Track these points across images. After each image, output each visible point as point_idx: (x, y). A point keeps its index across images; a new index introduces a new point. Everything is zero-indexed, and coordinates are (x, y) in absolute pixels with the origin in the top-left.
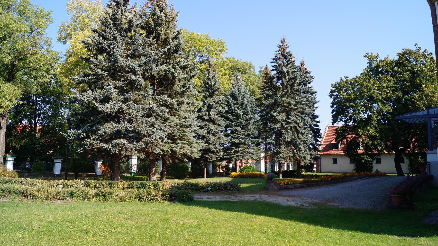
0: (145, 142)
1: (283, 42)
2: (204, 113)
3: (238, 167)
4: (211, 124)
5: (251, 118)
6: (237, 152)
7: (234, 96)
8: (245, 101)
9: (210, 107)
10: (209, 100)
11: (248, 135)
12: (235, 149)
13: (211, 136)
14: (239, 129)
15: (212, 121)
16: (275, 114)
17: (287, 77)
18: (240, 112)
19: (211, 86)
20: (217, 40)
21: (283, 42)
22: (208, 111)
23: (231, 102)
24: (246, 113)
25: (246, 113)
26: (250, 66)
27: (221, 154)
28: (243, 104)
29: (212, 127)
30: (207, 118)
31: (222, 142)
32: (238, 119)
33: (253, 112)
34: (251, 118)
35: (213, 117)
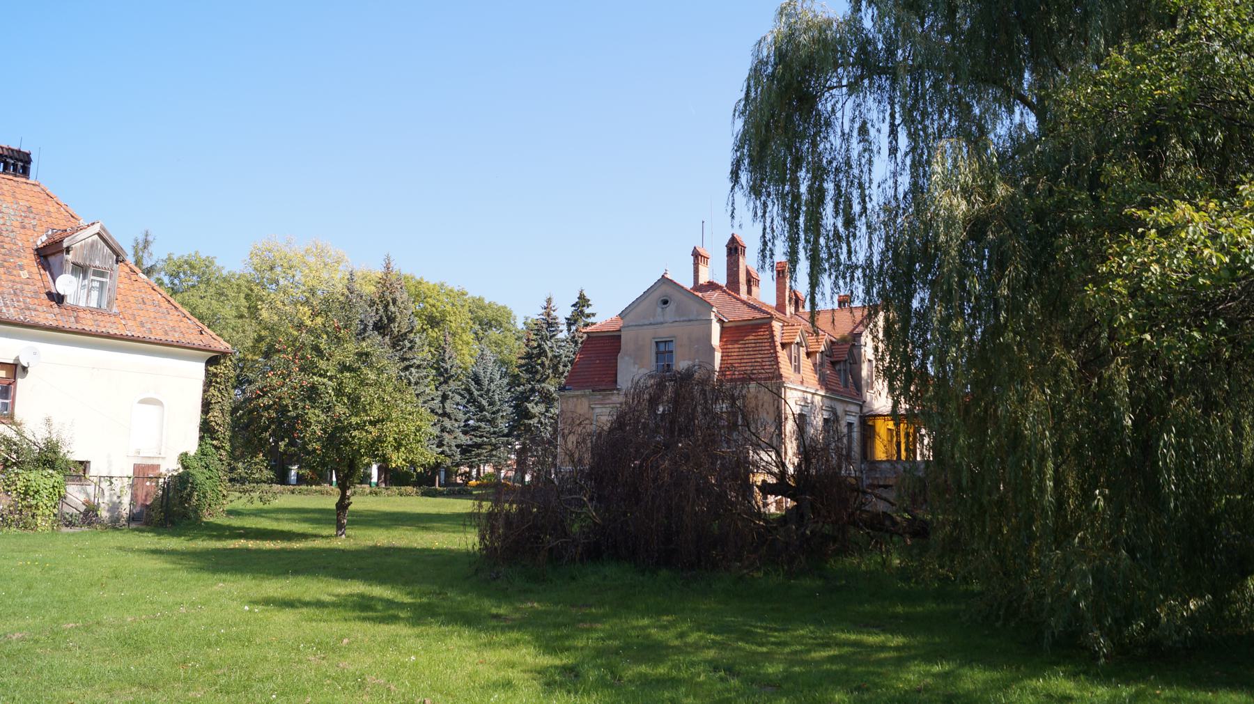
0: (77, 322)
1: (549, 301)
2: (436, 403)
3: (790, 426)
4: (446, 419)
5: (498, 411)
6: (478, 455)
7: (477, 380)
8: (493, 387)
9: (445, 397)
10: (445, 387)
11: (494, 433)
12: (476, 451)
13: (445, 434)
14: (483, 424)
15: (445, 414)
16: (529, 406)
17: (550, 355)
18: (484, 403)
19: (446, 370)
20: (456, 289)
21: (549, 301)
22: (443, 402)
23: (473, 387)
24: (492, 403)
25: (492, 403)
26: (509, 314)
27: (458, 457)
28: (489, 390)
29: (447, 423)
30: (440, 412)
31: (459, 442)
32: (481, 411)
33: (502, 401)
34: (498, 411)
35: (448, 410)
